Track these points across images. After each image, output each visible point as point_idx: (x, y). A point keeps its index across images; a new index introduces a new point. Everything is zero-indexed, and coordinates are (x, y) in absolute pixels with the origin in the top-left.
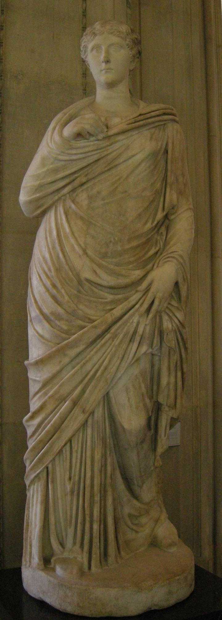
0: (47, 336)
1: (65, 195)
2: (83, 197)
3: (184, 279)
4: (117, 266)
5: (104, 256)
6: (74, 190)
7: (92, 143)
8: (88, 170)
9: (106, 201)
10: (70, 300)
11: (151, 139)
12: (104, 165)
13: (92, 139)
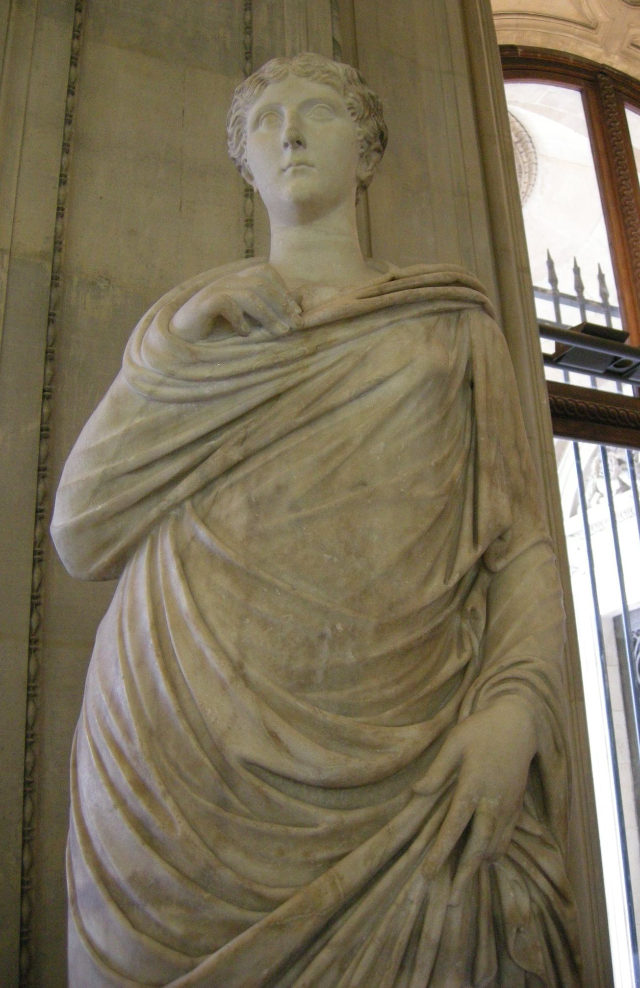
0: (120, 955)
1: (178, 504)
2: (232, 505)
3: (557, 748)
4: (345, 715)
5: (303, 683)
6: (206, 486)
7: (257, 348)
8: (247, 427)
9: (305, 512)
10: (193, 836)
11: (428, 339)
12: (296, 409)
13: (257, 334)
